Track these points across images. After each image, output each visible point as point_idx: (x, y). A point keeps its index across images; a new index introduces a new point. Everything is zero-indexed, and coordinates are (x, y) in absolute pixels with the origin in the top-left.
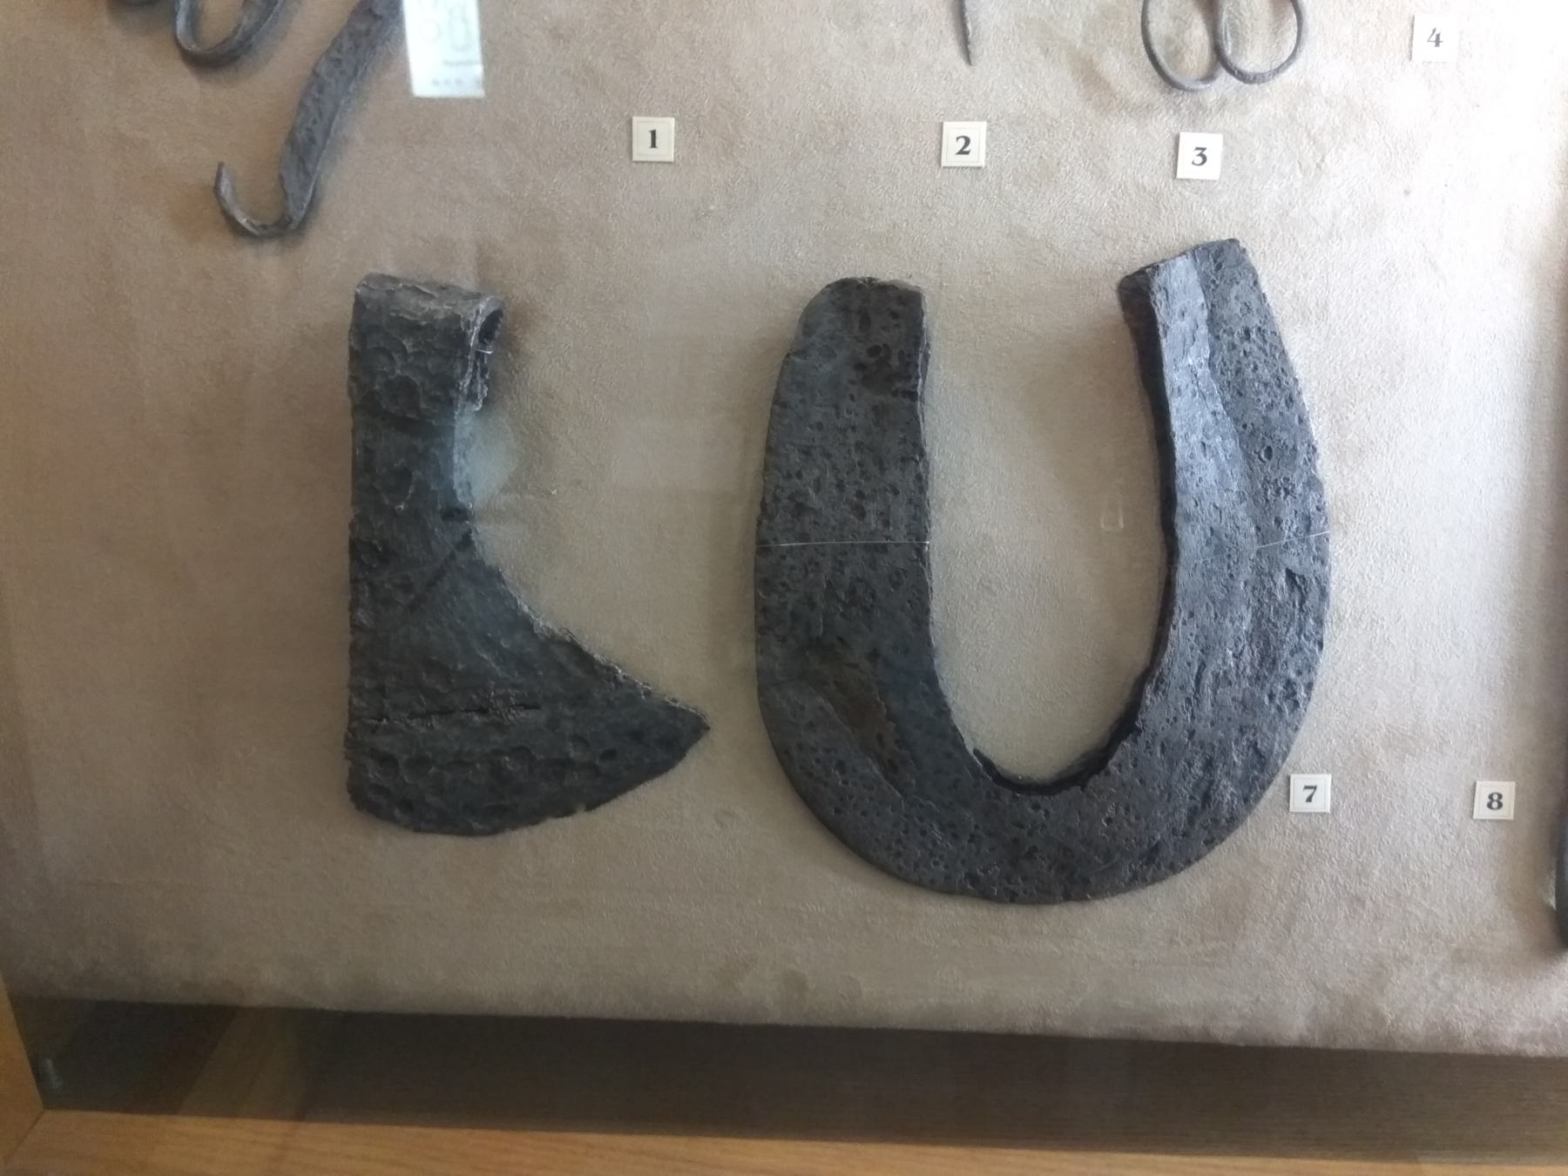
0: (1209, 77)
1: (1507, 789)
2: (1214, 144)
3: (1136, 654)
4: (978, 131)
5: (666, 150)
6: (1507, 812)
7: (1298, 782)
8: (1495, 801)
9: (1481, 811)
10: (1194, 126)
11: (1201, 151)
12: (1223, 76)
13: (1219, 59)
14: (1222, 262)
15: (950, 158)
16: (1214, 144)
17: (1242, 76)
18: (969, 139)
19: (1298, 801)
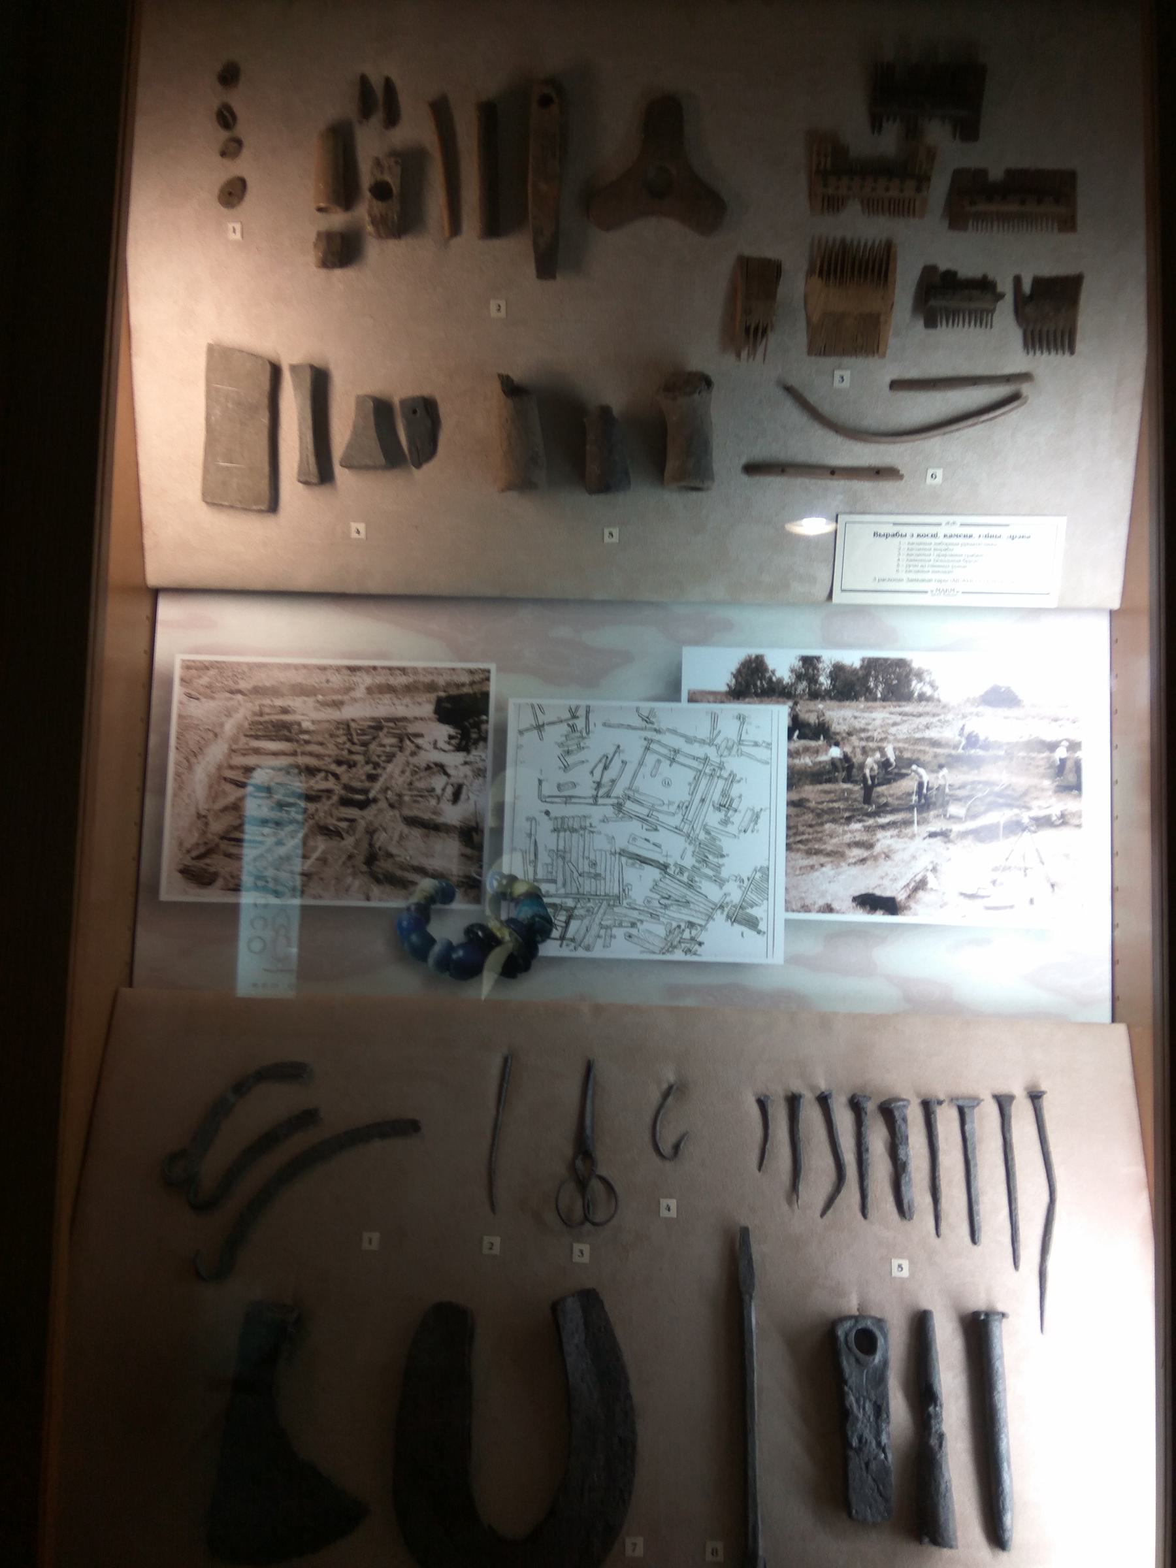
0: (582, 1224)
1: (719, 1546)
2: (586, 1248)
3: (967, 1127)
4: (497, 1241)
5: (375, 1246)
6: (720, 1558)
7: (629, 1542)
8: (714, 1552)
9: (709, 1557)
10: (579, 1241)
11: (611, 534)
12: (588, 1225)
13: (586, 1219)
14: (590, 1299)
15: (486, 1251)
16: (586, 1248)
17: (594, 1224)
18: (493, 1244)
19: (629, 1552)
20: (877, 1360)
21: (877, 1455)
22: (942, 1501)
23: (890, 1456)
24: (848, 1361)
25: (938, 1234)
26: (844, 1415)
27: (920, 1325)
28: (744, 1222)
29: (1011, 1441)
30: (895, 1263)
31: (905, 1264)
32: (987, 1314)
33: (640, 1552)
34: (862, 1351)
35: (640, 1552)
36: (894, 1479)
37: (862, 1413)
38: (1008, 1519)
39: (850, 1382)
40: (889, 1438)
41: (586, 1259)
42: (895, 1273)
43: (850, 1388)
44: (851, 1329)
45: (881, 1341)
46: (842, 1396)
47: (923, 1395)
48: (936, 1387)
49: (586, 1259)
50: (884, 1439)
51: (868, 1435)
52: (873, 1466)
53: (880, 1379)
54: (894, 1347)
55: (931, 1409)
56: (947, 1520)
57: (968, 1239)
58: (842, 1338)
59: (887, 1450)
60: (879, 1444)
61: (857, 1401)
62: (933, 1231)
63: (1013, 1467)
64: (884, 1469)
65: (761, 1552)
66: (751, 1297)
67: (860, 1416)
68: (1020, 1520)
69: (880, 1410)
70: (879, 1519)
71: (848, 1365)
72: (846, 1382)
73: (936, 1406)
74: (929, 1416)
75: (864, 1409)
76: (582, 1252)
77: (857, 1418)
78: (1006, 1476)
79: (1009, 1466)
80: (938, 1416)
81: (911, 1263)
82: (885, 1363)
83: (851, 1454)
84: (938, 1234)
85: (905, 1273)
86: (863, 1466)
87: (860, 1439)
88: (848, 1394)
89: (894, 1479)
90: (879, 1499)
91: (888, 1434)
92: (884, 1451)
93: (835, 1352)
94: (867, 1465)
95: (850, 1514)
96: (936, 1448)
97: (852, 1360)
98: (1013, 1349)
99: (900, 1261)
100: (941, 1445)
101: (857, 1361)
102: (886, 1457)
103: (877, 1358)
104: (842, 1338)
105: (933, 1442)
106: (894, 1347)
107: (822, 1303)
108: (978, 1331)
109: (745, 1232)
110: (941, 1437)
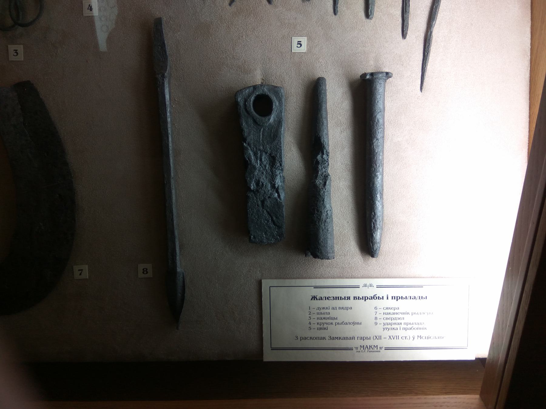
1: (149, 266)
2: (20, 48)
6: (150, 275)
7: (76, 268)
8: (145, 271)
9: (141, 275)
17: (22, 25)
19: (77, 275)
20: (272, 120)
21: (271, 194)
22: (322, 226)
23: (282, 196)
24: (247, 123)
25: (335, 12)
26: (245, 166)
27: (314, 92)
28: (158, 15)
29: (386, 178)
30: (295, 40)
31: (304, 41)
32: (372, 74)
33: (86, 274)
34: (260, 115)
35: (86, 274)
36: (286, 211)
37: (259, 164)
38: (378, 235)
39: (248, 140)
40: (283, 179)
41: (21, 57)
42: (295, 49)
43: (249, 144)
44: (249, 96)
45: (276, 104)
46: (243, 150)
47: (313, 146)
48: (324, 139)
49: (21, 57)
50: (278, 182)
51: (264, 180)
52: (268, 203)
53: (274, 135)
54: (291, 110)
55: (319, 157)
56: (326, 239)
57: (362, 14)
58: (242, 104)
59: (281, 191)
60: (273, 186)
61: (255, 154)
62: (331, 9)
63: (385, 197)
64: (278, 205)
65: (179, 270)
66: (163, 76)
67: (258, 166)
68: (385, 237)
69: (275, 160)
70: (273, 241)
71: (246, 125)
72: (245, 140)
73: (323, 154)
74: (318, 163)
75: (261, 160)
76: (17, 52)
77: (255, 168)
78: (378, 204)
79: (382, 197)
80: (325, 162)
81: (310, 39)
82: (279, 122)
83: (250, 195)
84: (335, 12)
85: (304, 49)
86: (260, 203)
87: (257, 183)
88: (247, 149)
89: (286, 211)
90: (272, 225)
91: (283, 179)
92: (277, 192)
93: (241, 119)
94: (263, 202)
95: (247, 233)
96: (321, 186)
97: (250, 121)
98: (394, 106)
99: (300, 39)
100: (325, 184)
101: (255, 122)
102: (279, 196)
103: (272, 119)
104: (242, 104)
105: (319, 181)
106: (291, 110)
107: (229, 78)
108: (364, 93)
109: (158, 22)
110: (326, 177)
